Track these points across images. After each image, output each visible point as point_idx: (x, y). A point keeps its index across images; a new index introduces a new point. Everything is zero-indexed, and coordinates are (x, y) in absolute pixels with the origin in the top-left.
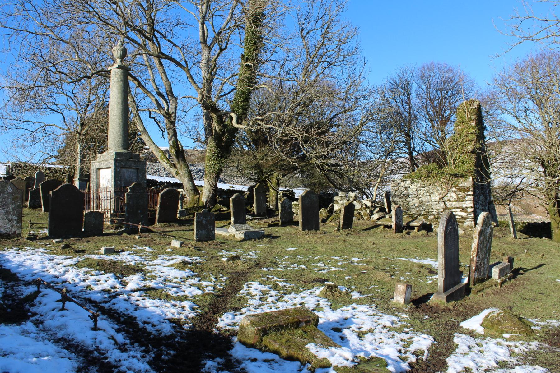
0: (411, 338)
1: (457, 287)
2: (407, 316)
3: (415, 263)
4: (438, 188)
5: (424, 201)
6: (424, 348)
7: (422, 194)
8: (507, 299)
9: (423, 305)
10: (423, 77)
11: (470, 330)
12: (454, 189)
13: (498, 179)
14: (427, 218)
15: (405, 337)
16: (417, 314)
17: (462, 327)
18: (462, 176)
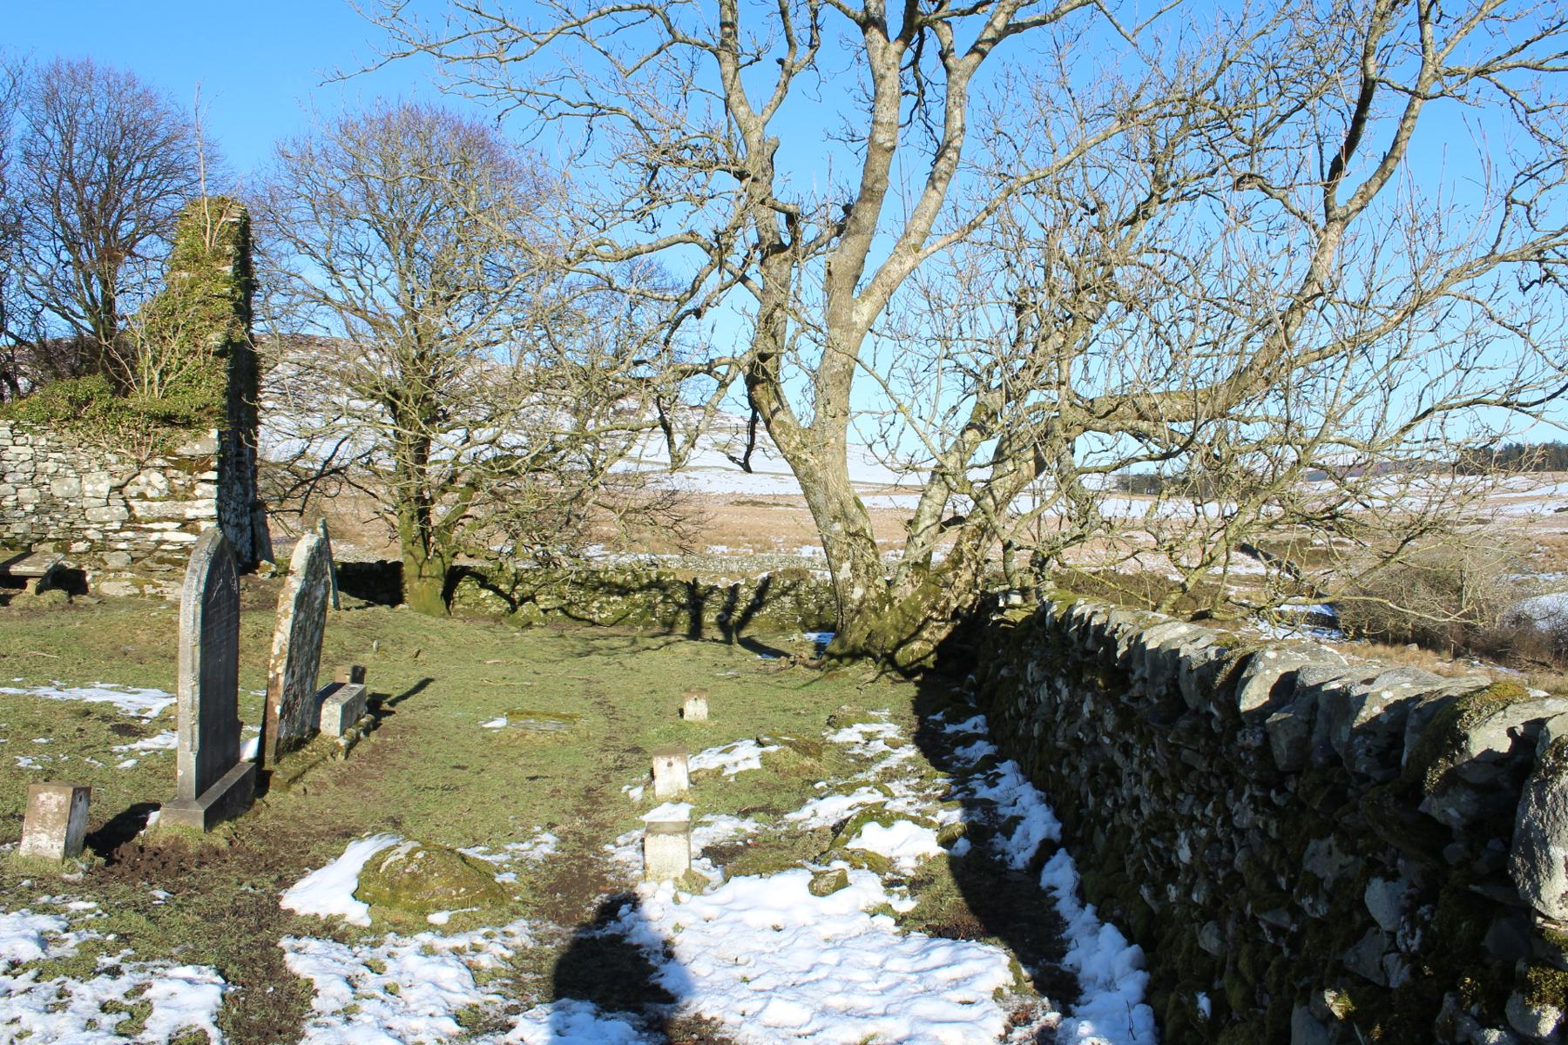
0: (139, 990)
1: (233, 776)
2: (92, 905)
3: (55, 702)
4: (108, 456)
5: (58, 493)
6: (204, 1021)
7: (50, 471)
8: (377, 795)
9: (125, 849)
10: (51, 99)
11: (323, 916)
12: (159, 462)
13: (277, 440)
14: (66, 550)
15: (114, 990)
16: (123, 888)
17: (291, 912)
18: (188, 424)
